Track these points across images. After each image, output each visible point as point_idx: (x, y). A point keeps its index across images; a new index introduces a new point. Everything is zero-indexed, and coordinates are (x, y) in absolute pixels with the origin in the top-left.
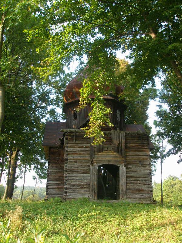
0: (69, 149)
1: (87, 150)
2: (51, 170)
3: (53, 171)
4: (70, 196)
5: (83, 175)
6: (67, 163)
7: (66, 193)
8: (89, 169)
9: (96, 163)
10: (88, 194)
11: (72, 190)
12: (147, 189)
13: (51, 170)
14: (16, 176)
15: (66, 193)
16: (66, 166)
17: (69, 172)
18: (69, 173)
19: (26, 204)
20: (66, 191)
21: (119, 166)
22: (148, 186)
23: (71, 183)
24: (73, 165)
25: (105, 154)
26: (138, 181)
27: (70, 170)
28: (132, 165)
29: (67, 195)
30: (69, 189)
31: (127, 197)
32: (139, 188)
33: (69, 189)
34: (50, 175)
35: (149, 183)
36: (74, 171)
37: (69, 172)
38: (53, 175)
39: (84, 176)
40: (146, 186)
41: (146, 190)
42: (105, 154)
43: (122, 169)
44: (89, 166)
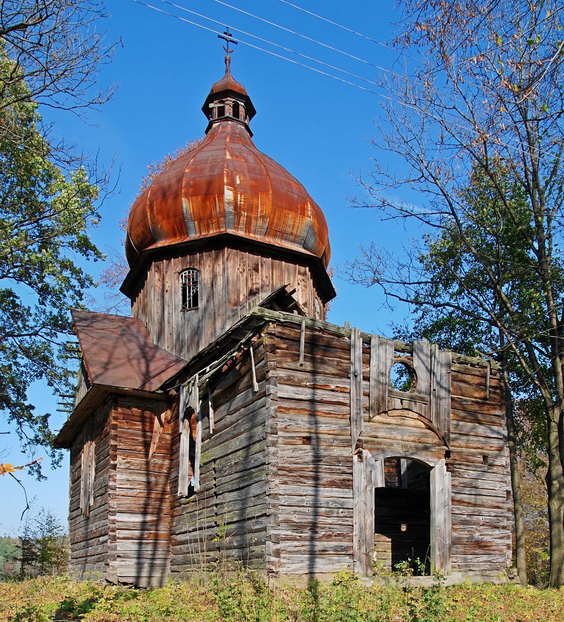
0: (282, 391)
1: (342, 400)
2: (124, 477)
3: (131, 478)
4: (293, 566)
5: (332, 491)
6: (274, 444)
7: (277, 553)
8: (350, 471)
9: (370, 450)
10: (347, 558)
11: (296, 543)
12: (499, 541)
13: (124, 477)
14: (558, 440)
15: (277, 553)
16: (274, 454)
17: (286, 479)
18: (285, 483)
19: (261, 591)
20: (278, 546)
21: (432, 465)
22: (503, 531)
23: (294, 519)
24: (297, 454)
25: (393, 421)
26: (481, 518)
27: (290, 471)
28: (467, 465)
29: (283, 561)
30: (287, 539)
31: (453, 567)
32: (481, 537)
33: (287, 539)
34: (122, 493)
35: (505, 525)
36: (301, 476)
37: (286, 479)
38: (130, 492)
39: (333, 494)
40: (497, 532)
41: (497, 545)
42: (393, 421)
43: (441, 482)
44: (349, 461)
